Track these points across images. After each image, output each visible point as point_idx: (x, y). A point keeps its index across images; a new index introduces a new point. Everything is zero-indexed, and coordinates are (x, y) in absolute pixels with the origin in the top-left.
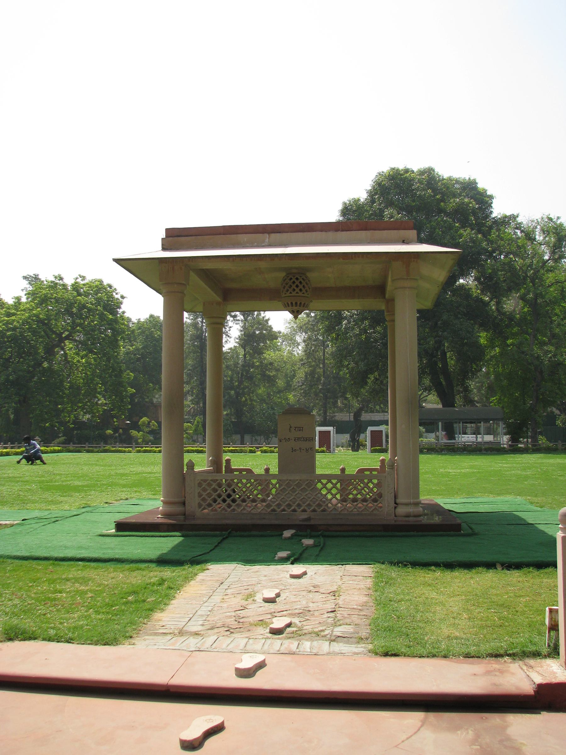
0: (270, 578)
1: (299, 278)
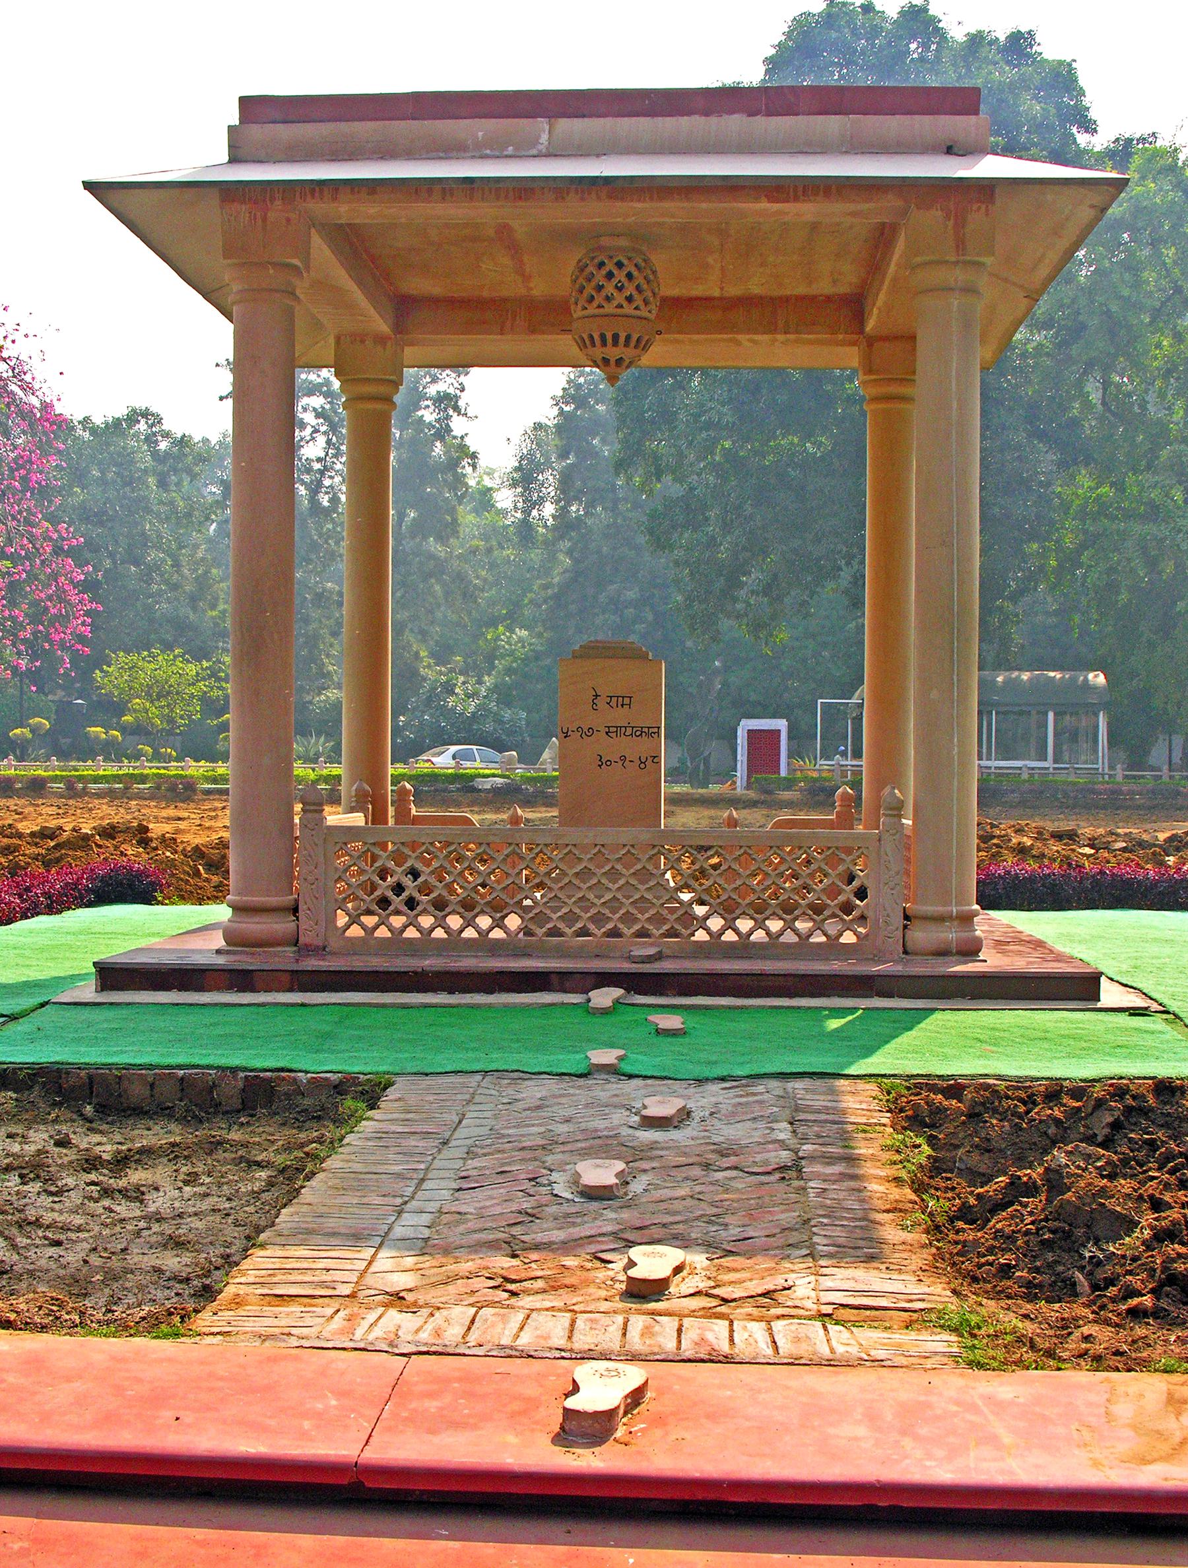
0: (583, 1126)
1: (625, 262)
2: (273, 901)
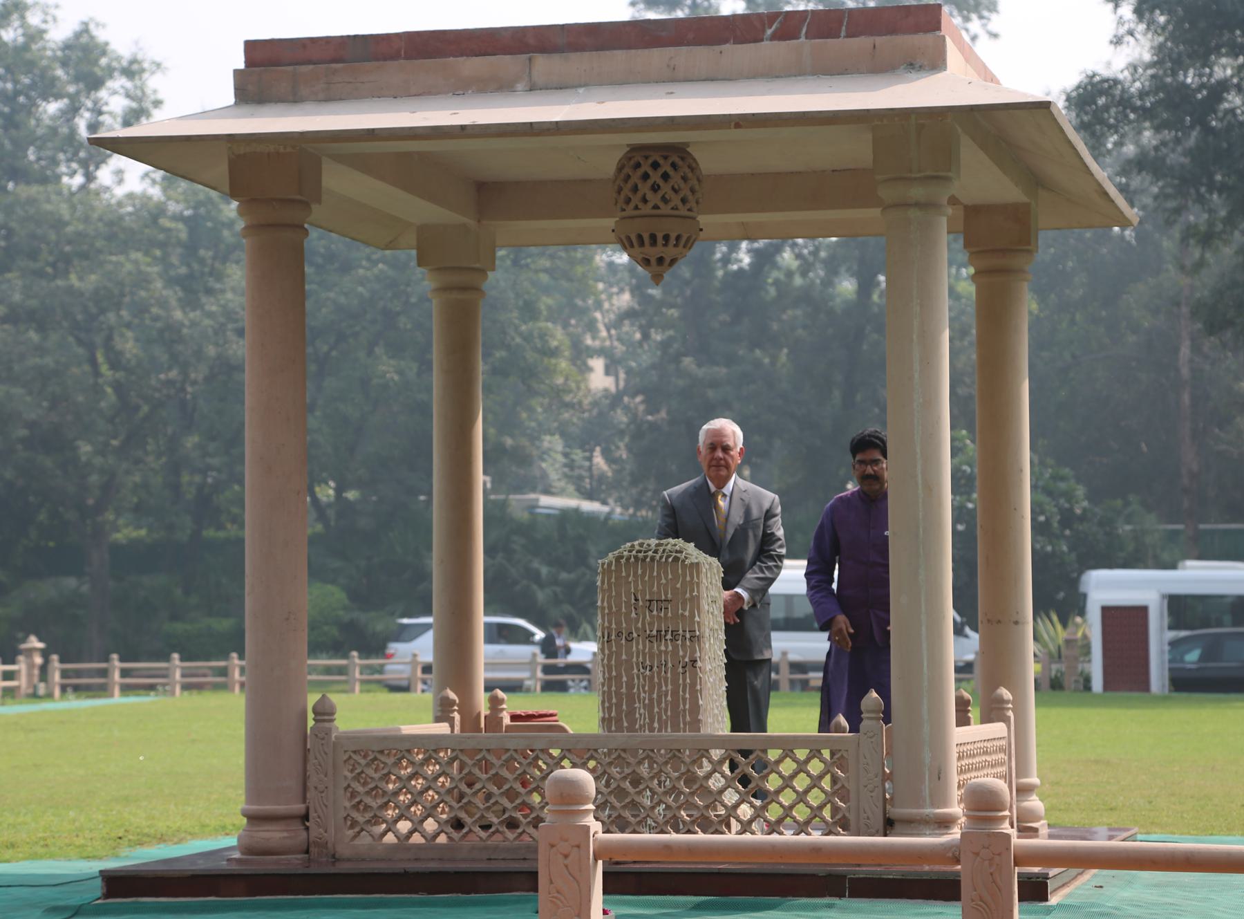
2: (281, 808)
